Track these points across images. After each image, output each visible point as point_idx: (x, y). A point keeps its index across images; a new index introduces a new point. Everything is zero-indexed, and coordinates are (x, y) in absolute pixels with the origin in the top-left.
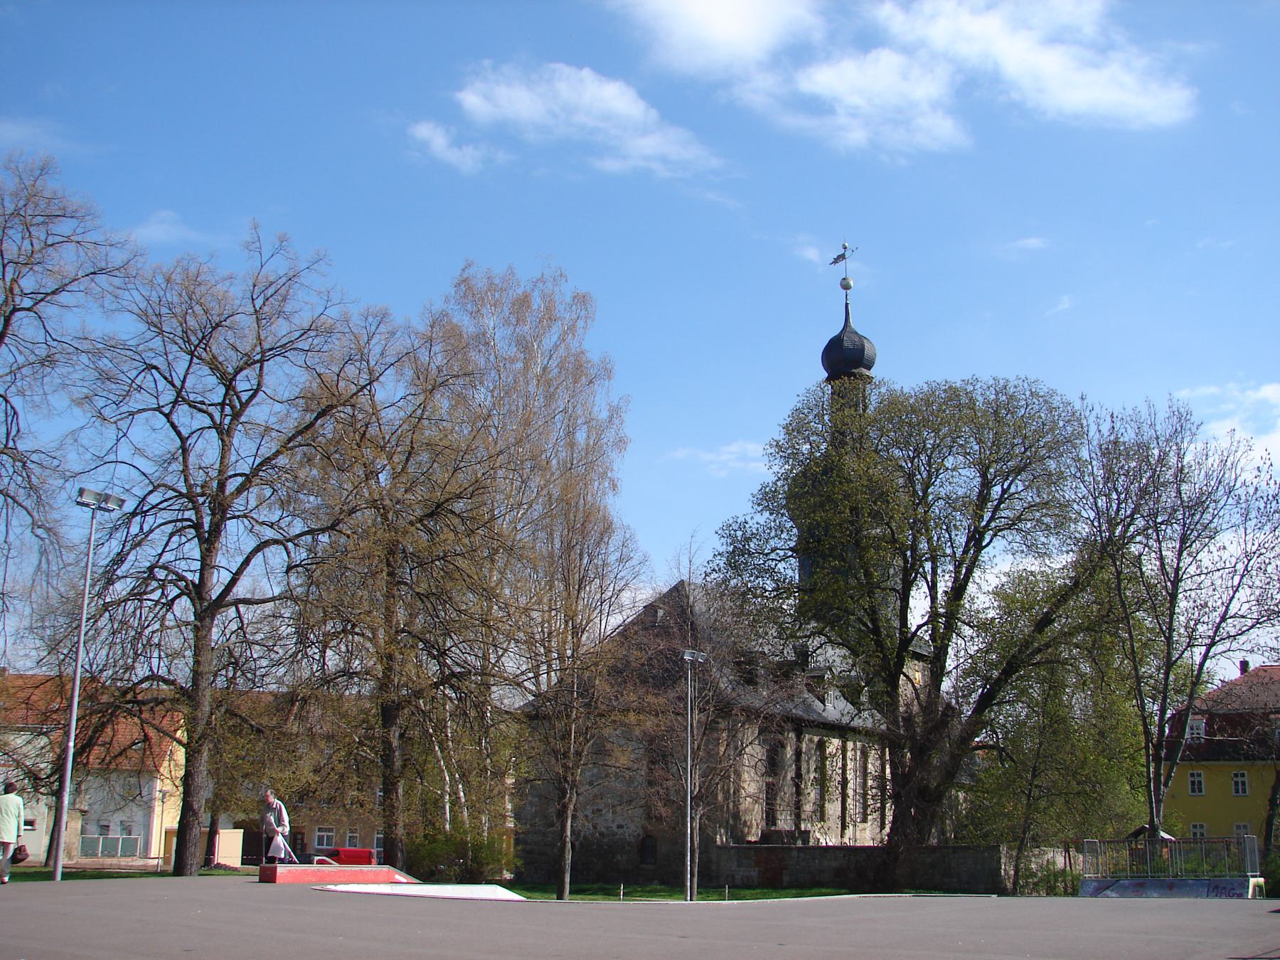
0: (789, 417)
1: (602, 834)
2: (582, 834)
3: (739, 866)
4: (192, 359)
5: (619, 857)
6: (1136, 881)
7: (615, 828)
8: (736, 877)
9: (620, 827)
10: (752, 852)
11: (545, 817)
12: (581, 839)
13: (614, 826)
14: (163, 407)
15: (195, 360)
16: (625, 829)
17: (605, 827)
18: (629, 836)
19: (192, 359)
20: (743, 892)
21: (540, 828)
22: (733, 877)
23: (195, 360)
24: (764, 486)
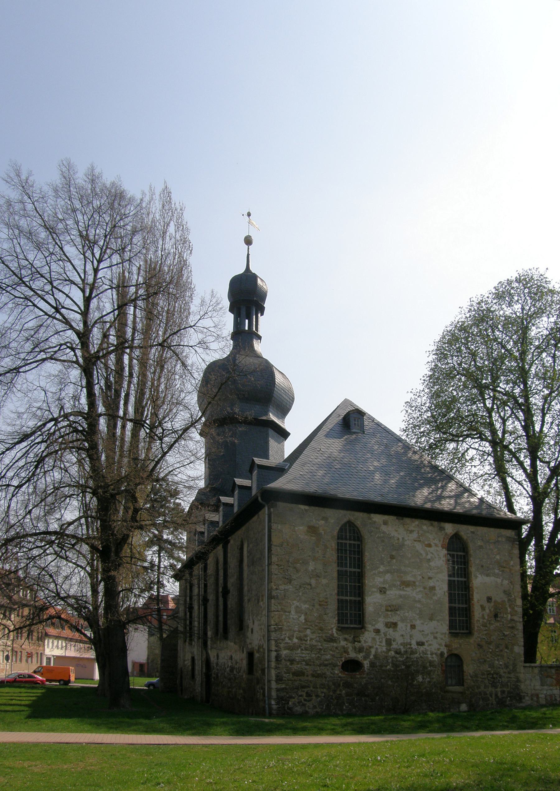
0: (423, 376)
1: (397, 652)
2: (373, 651)
3: (542, 685)
4: (120, 263)
5: (420, 678)
6: (233, 631)
7: (414, 646)
8: (540, 696)
9: (420, 644)
10: (553, 671)
11: (321, 629)
12: (372, 657)
13: (414, 643)
14: (109, 289)
15: (121, 265)
16: (426, 647)
17: (401, 644)
18: (432, 654)
19: (120, 263)
20: (321, 722)
21: (314, 643)
22: (537, 696)
23: (121, 265)
24: (261, 310)
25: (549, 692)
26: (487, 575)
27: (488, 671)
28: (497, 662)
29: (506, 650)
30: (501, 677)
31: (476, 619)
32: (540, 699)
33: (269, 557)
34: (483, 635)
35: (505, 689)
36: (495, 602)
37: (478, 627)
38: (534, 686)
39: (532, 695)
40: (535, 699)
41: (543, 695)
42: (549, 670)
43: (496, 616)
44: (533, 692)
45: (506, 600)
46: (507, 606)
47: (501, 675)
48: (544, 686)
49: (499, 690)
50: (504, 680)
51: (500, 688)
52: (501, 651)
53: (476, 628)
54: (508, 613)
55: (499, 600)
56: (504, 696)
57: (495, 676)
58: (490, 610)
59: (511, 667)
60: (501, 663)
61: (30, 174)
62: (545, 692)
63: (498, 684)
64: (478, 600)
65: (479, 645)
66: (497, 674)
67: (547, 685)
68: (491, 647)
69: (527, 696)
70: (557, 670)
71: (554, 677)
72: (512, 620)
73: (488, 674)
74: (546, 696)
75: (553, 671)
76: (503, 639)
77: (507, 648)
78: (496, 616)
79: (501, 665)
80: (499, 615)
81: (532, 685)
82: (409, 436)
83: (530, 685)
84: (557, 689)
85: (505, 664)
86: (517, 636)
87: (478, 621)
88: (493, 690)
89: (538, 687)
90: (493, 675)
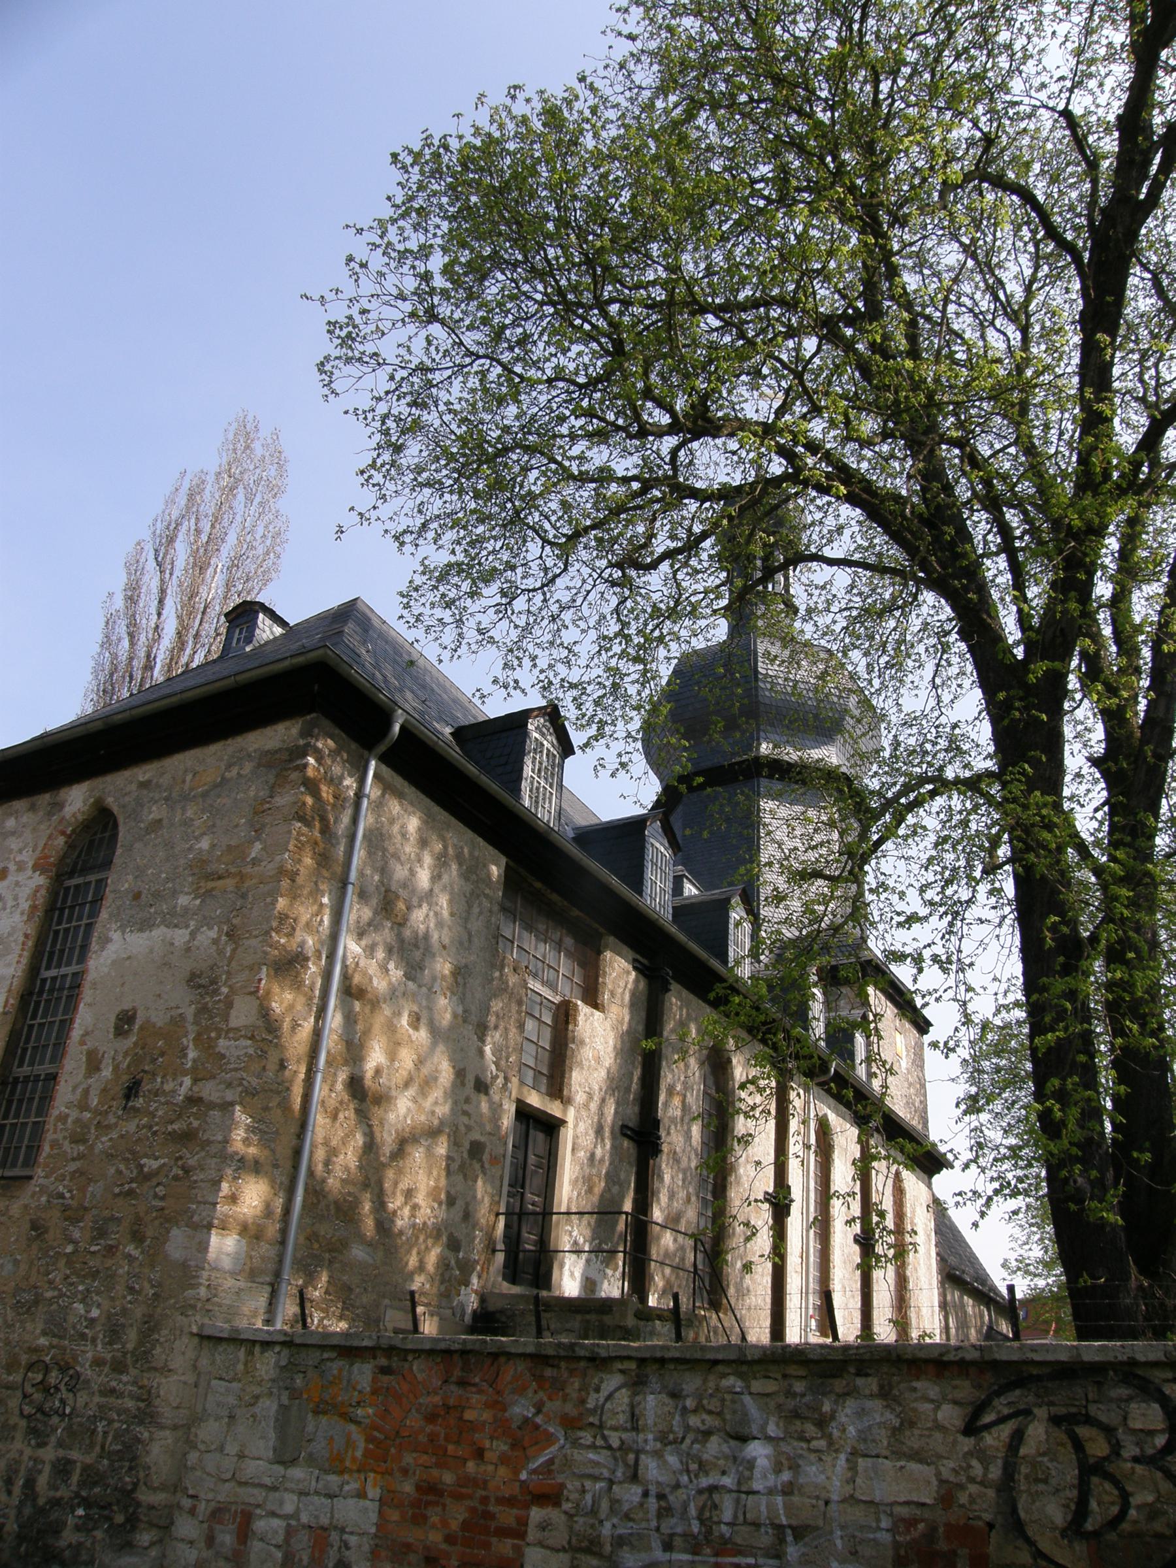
3: (284, 1458)
22: (245, 1521)
25: (315, 1511)
26: (145, 925)
27: (36, 1350)
28: (79, 1307)
29: (131, 1249)
30: (75, 1383)
31: (55, 1113)
32: (256, 1546)
33: (284, 1231)
34: (62, 1178)
35: (75, 1455)
36: (147, 1026)
37: (55, 1144)
38: (241, 1456)
39: (217, 1514)
40: (227, 1539)
41: (276, 1523)
42: (336, 1367)
43: (132, 1090)
44: (225, 1492)
45: (190, 1012)
46: (188, 1041)
47: (78, 1375)
48: (293, 1462)
49: (49, 1454)
50: (85, 1402)
51: (60, 1444)
52: (111, 1250)
53: (46, 1149)
54: (185, 1073)
55: (159, 1019)
56: (63, 1492)
57: (54, 1377)
58: (116, 1068)
59: (131, 1337)
60: (95, 1313)
61: (276, 435)
62: (290, 1504)
63: (55, 1420)
64: (87, 1034)
65: (35, 1226)
66: (64, 1368)
67: (311, 1460)
68: (77, 1234)
69: (192, 1512)
70: (385, 1370)
71: (366, 1412)
72: (193, 1100)
73: (30, 1367)
74: (289, 1532)
75: (363, 1374)
76: (130, 1193)
77: (137, 1237)
78: (132, 1090)
79: (92, 1322)
80: (146, 1087)
81: (232, 1449)
82: (520, 604)
83: (221, 1449)
84: (361, 1495)
85: (109, 1317)
86: (198, 1176)
87: (63, 1118)
88: (28, 1452)
89: (258, 1468)
90: (47, 1370)
